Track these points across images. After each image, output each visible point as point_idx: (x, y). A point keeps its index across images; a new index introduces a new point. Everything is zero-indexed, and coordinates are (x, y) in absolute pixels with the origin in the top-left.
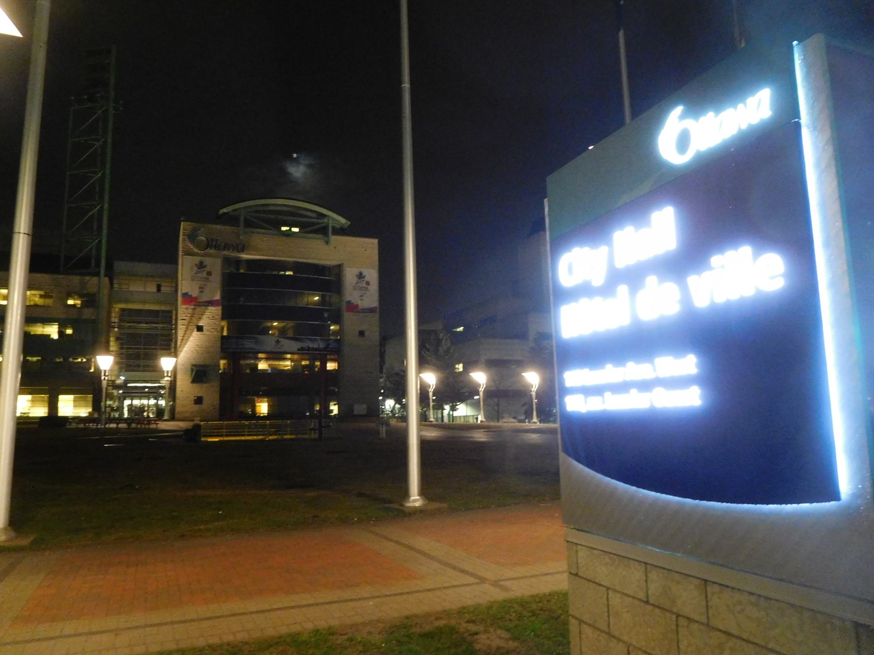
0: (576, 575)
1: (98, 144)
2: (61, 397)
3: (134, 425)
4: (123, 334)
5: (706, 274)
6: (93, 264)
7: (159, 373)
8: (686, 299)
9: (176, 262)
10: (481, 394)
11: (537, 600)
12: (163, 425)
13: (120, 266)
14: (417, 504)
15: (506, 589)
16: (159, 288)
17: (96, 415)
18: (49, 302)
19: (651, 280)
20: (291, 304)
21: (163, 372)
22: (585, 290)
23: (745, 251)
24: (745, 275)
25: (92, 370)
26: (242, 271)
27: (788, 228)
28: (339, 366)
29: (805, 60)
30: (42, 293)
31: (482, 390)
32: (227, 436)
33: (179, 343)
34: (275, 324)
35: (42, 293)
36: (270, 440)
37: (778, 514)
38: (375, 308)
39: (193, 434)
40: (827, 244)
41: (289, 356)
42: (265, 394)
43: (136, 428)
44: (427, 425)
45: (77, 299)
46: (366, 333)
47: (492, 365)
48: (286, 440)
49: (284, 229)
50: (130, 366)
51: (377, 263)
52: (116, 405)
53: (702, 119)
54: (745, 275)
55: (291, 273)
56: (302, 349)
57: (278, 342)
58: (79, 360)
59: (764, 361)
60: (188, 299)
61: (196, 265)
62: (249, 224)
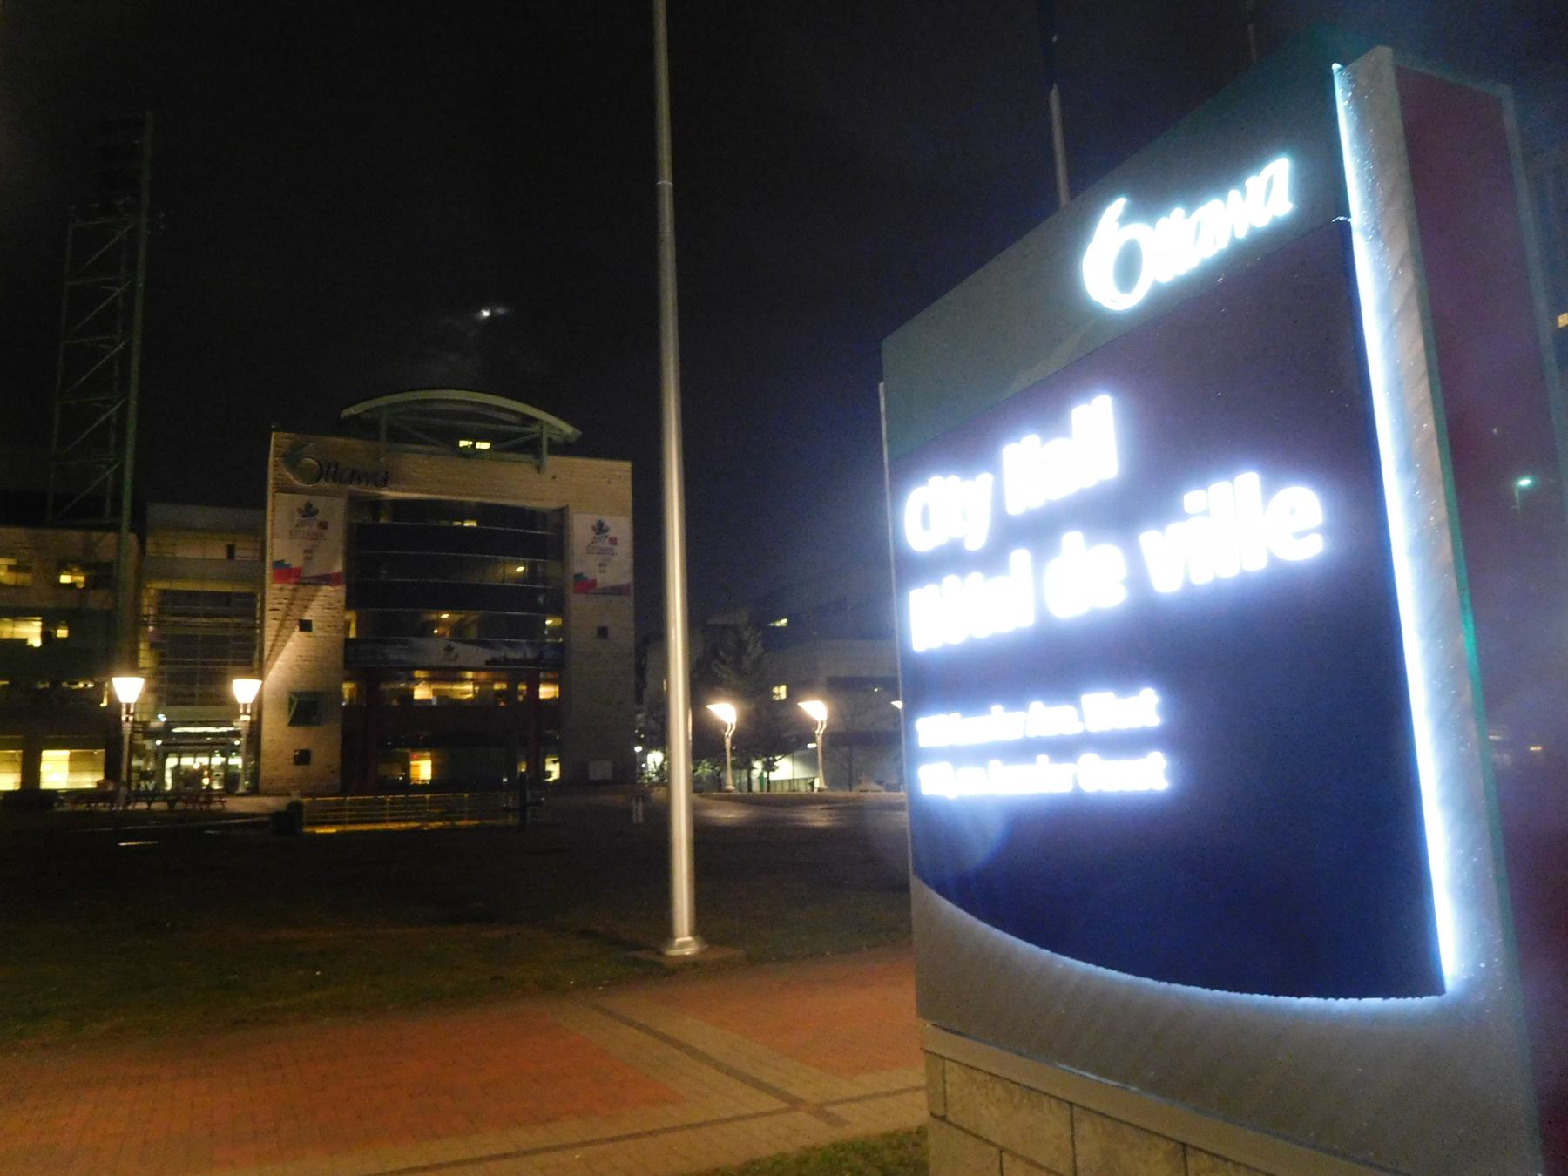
0: (943, 1118)
1: (117, 291)
2: (46, 754)
3: (179, 806)
4: (164, 637)
5: (1174, 528)
6: (108, 510)
7: (230, 709)
8: (1138, 579)
9: (261, 505)
10: (819, 739)
11: (895, 1143)
12: (235, 805)
13: (158, 512)
14: (688, 952)
15: (837, 1122)
16: (231, 551)
17: (110, 788)
18: (24, 578)
19: (1072, 540)
20: (474, 579)
21: (236, 705)
22: (952, 560)
23: (1248, 481)
24: (1251, 528)
25: (104, 704)
26: (382, 521)
27: (1331, 436)
28: (561, 692)
29: (1356, 101)
30: (12, 562)
31: (819, 732)
32: (351, 823)
33: (266, 653)
34: (445, 616)
35: (12, 562)
36: (432, 831)
37: (1321, 1016)
38: (628, 586)
39: (288, 820)
40: (1408, 462)
41: (470, 675)
42: (420, 745)
43: (185, 810)
44: (720, 799)
45: (78, 573)
46: (612, 632)
47: (839, 687)
48: (459, 829)
49: (463, 443)
50: (176, 695)
51: (630, 505)
52: (151, 766)
53: (1163, 222)
54: (1251, 528)
55: (474, 524)
56: (494, 661)
57: (449, 649)
58: (81, 685)
59: (1292, 700)
60: (284, 572)
61: (299, 510)
62: (398, 436)
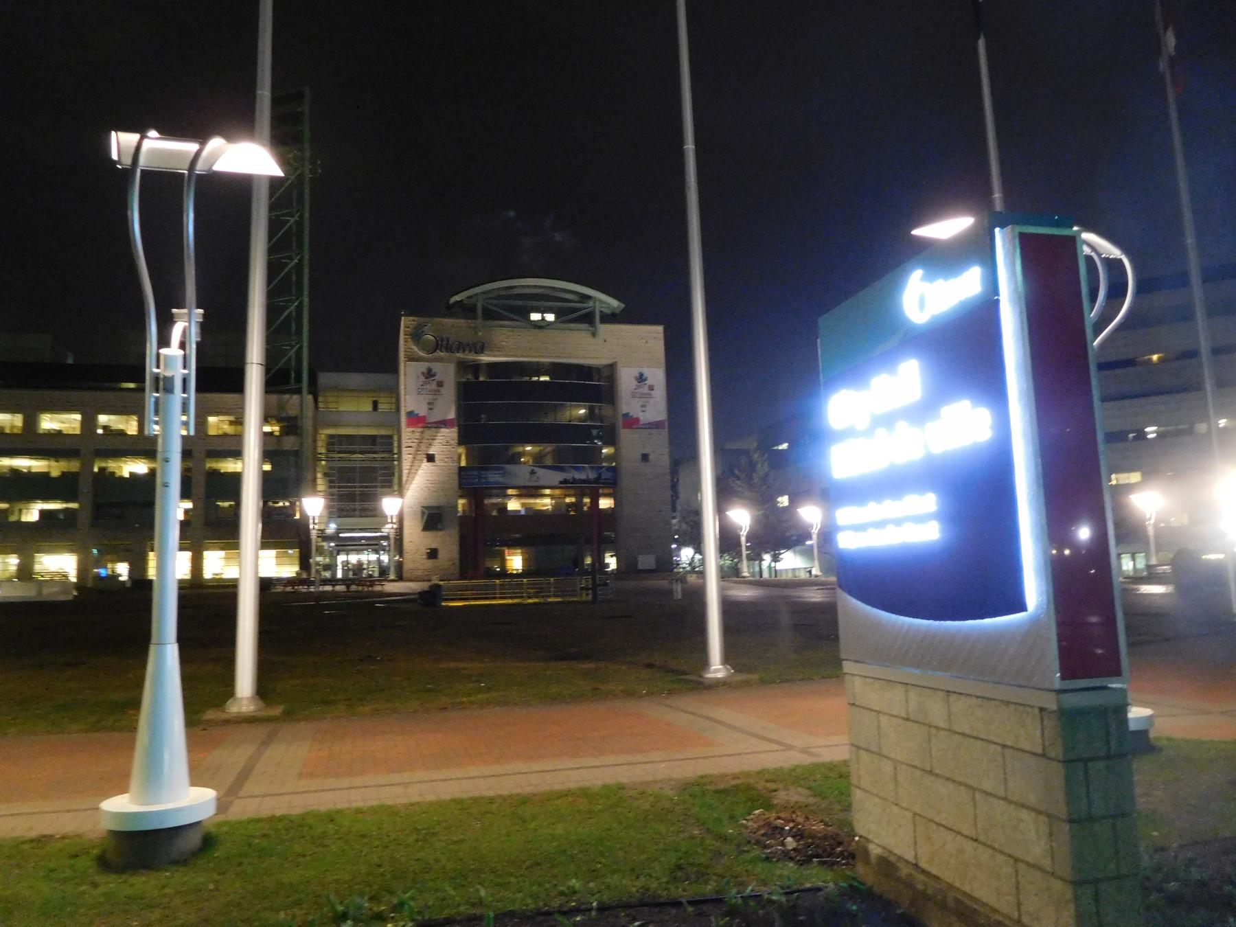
42: (513, 544)
46: (651, 457)
57: (533, 472)
62: (489, 315)
